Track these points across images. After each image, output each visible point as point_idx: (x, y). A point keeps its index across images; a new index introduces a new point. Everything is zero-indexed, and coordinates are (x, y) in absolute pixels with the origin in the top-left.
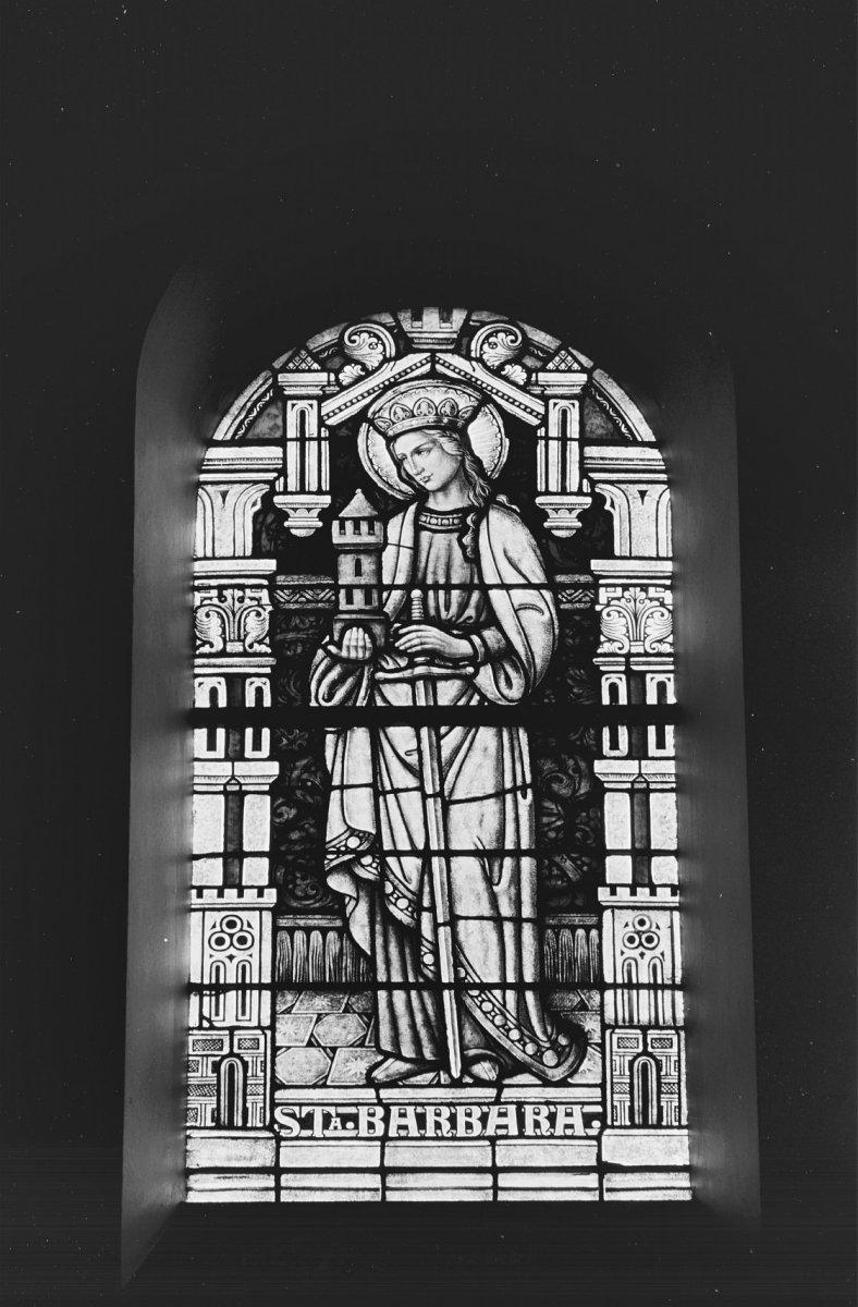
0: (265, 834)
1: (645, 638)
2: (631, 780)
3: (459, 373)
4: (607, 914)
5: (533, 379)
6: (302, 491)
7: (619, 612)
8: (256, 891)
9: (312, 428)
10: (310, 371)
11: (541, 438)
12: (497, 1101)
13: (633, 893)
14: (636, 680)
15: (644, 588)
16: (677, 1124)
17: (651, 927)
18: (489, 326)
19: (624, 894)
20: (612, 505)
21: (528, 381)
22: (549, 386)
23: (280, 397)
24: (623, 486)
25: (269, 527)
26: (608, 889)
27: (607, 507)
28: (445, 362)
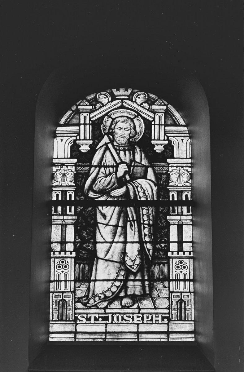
0: (68, 238)
1: (182, 181)
2: (178, 221)
3: (133, 107)
4: (171, 260)
5: (151, 107)
6: (85, 139)
7: (175, 174)
8: (70, 253)
9: (87, 122)
10: (87, 105)
11: (153, 125)
12: (139, 313)
13: (178, 254)
14: (180, 193)
15: (67, 166)
16: (190, 320)
17: (66, 263)
18: (136, 94)
19: (175, 254)
20: (174, 143)
21: (149, 108)
22: (155, 109)
23: (78, 112)
24: (177, 138)
25: (75, 149)
26: (171, 253)
27: (172, 144)
28: (126, 102)
